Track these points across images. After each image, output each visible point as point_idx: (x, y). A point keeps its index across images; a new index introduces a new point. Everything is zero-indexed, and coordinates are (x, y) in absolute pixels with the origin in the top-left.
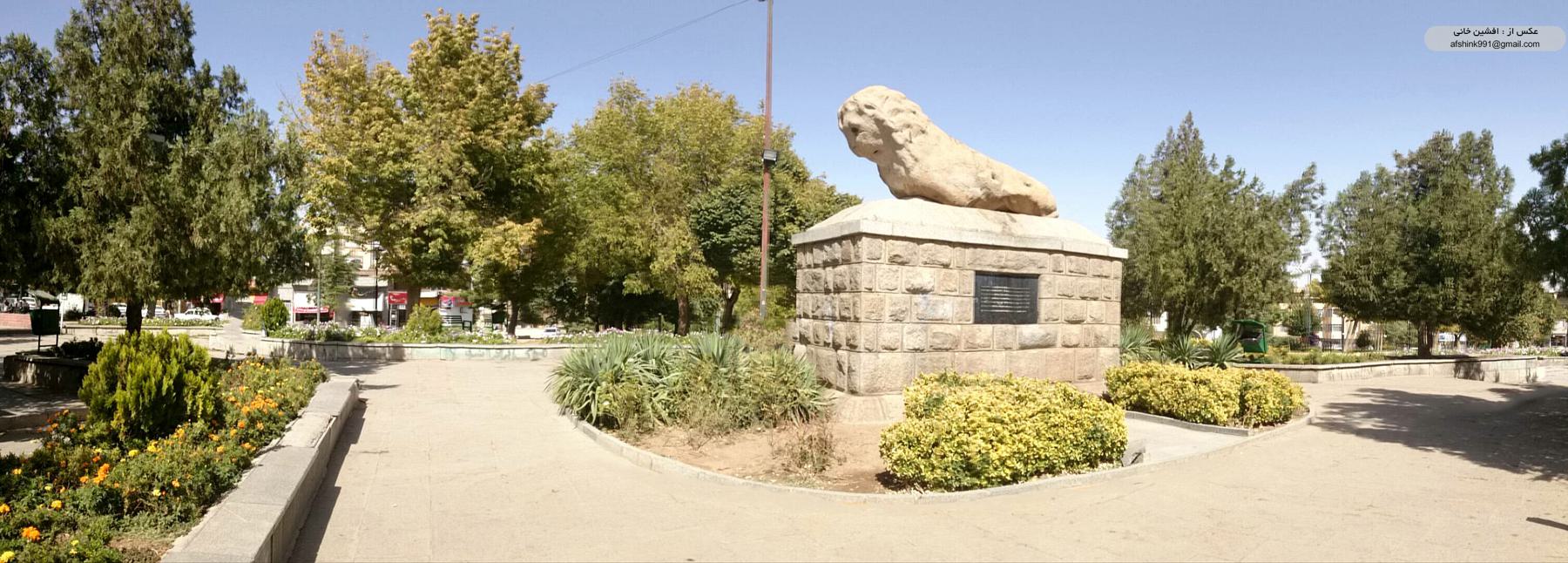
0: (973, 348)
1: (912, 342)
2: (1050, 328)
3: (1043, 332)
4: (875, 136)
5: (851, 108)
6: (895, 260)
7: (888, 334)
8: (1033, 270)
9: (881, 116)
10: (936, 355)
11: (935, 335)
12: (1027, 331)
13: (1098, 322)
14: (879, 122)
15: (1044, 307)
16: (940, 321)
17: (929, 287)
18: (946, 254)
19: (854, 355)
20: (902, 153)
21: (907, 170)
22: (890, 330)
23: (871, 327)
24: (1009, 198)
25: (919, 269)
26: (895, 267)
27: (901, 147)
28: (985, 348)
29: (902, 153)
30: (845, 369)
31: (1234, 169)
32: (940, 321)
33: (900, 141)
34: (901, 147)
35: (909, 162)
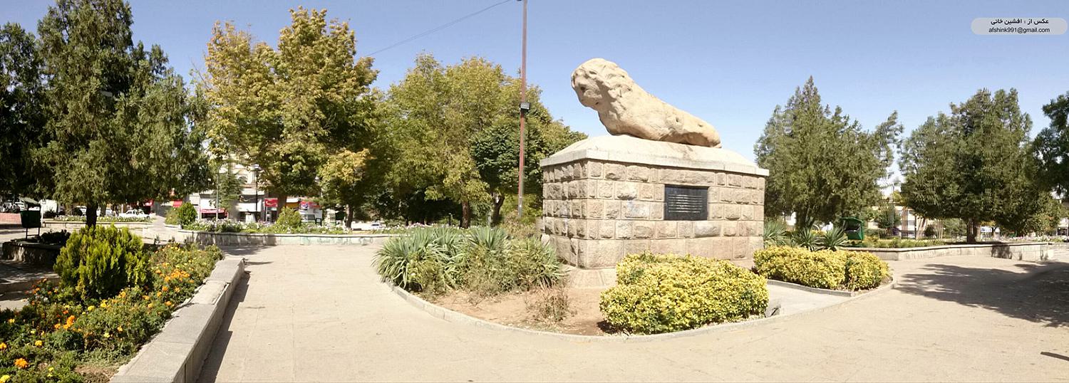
0: (663, 237)
1: (621, 232)
2: (716, 223)
3: (711, 226)
4: (597, 92)
5: (580, 73)
6: (610, 177)
7: (606, 227)
8: (704, 184)
9: (601, 79)
10: (638, 242)
11: (637, 228)
12: (701, 225)
13: (748, 219)
14: (599, 83)
15: (712, 209)
16: (641, 218)
17: (633, 195)
18: (645, 173)
19: (582, 241)
20: (615, 104)
21: (619, 116)
22: (607, 224)
23: (594, 222)
24: (688, 134)
25: (626, 183)
26: (610, 182)
27: (614, 100)
28: (672, 237)
29: (615, 104)
30: (576, 251)
31: (841, 115)
32: (641, 218)
33: (614, 96)
34: (614, 100)
35: (620, 110)
